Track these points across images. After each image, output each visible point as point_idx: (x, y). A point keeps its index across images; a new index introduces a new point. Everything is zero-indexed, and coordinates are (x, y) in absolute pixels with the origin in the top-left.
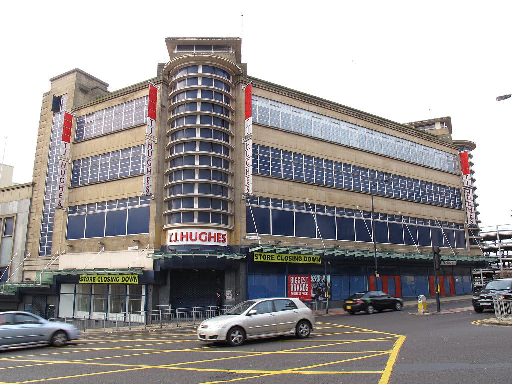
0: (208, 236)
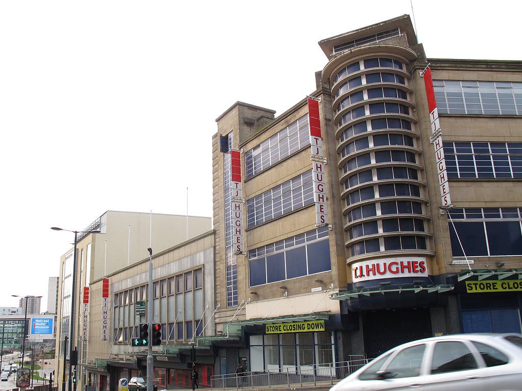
0: (399, 266)
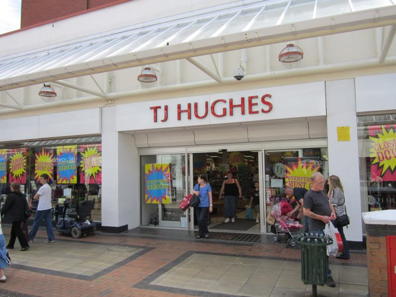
0: (227, 106)
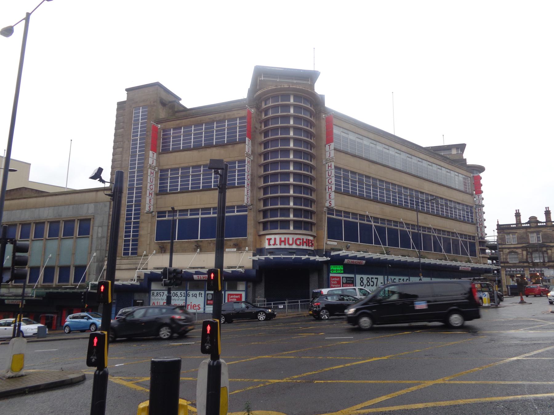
0: (301, 241)
